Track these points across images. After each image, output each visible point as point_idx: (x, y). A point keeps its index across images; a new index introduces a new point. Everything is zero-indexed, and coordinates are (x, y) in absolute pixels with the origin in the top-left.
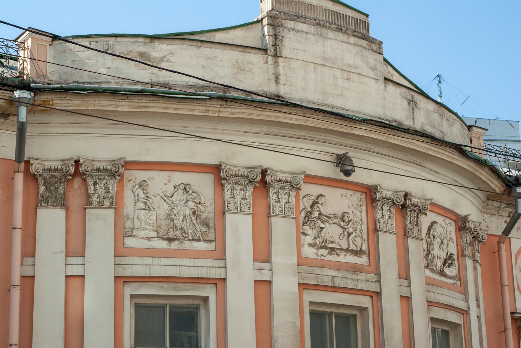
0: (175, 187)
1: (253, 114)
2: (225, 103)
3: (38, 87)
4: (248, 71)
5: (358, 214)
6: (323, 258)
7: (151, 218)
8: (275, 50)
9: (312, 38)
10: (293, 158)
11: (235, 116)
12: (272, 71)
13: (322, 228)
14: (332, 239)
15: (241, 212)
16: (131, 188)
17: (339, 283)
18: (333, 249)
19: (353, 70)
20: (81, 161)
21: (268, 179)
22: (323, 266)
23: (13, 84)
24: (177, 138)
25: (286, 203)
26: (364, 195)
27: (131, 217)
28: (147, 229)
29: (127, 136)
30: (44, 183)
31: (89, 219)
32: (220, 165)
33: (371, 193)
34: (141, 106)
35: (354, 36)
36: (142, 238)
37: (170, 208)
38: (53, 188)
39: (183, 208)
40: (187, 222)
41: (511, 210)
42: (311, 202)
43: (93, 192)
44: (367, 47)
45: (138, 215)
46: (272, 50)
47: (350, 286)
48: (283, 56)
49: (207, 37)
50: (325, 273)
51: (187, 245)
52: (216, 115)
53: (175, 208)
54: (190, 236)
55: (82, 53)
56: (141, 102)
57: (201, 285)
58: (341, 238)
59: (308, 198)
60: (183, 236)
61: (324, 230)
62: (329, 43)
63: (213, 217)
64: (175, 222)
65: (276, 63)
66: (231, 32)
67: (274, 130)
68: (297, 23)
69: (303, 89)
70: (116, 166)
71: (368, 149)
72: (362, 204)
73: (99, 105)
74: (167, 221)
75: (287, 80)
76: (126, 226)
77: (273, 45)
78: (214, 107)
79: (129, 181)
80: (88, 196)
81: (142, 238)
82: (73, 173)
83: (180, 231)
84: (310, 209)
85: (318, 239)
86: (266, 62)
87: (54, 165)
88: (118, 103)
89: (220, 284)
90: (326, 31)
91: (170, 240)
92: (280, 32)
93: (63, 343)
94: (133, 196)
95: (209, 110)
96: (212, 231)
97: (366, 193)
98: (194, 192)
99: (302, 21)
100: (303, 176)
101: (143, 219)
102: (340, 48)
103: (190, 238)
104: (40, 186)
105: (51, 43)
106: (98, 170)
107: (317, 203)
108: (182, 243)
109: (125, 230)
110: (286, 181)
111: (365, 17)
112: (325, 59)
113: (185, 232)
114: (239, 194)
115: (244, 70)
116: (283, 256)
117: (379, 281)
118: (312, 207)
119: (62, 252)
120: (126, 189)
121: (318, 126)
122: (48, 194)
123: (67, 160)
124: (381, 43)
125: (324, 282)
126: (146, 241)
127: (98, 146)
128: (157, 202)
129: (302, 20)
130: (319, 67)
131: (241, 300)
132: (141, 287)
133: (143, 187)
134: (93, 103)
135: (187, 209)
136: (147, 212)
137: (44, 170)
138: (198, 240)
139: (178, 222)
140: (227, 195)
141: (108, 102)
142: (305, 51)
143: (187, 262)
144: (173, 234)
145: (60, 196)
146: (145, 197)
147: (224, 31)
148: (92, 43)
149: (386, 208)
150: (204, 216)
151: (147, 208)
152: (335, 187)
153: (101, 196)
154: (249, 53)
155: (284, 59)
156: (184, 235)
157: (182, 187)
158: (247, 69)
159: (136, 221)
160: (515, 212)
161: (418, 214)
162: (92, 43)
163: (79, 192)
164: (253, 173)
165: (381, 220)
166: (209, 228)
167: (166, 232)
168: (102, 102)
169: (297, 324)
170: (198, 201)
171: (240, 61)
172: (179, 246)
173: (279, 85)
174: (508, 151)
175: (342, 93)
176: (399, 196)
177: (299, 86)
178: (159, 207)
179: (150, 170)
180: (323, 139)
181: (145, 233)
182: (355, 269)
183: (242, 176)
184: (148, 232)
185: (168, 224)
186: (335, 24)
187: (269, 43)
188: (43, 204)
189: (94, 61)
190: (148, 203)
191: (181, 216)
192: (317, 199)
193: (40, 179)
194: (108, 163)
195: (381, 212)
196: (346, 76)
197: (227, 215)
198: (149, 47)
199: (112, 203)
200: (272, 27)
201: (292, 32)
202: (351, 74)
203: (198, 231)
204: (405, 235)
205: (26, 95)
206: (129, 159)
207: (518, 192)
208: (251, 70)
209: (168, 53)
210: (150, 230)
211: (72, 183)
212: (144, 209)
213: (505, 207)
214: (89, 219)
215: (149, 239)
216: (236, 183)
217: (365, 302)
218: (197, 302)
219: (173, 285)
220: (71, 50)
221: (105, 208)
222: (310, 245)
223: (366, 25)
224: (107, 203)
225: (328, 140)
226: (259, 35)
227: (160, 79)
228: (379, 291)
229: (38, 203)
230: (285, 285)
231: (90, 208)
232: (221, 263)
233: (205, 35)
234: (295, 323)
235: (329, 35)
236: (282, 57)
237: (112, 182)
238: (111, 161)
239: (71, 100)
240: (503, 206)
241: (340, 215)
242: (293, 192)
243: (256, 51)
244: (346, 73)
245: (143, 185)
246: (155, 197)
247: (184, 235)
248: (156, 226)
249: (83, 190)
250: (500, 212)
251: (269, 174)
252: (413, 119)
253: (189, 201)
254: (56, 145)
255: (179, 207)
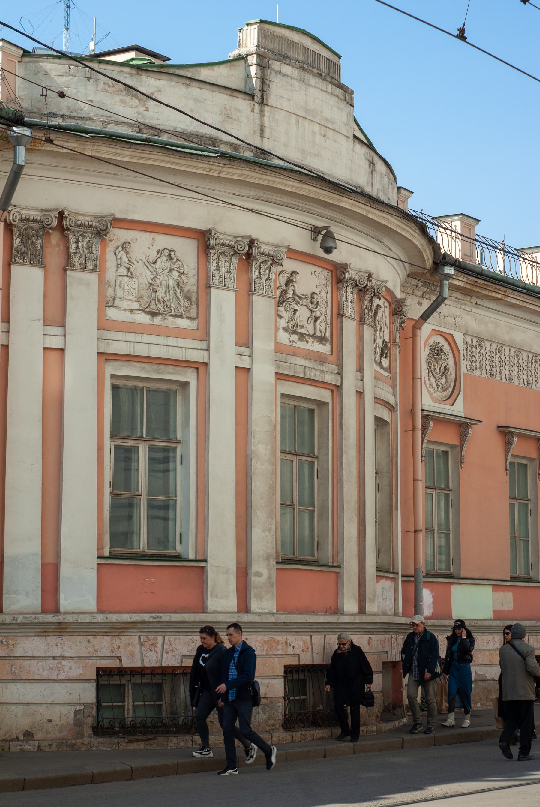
0: (158, 252)
1: (253, 177)
2: (229, 163)
3: (33, 123)
4: (235, 120)
5: (324, 295)
6: (295, 345)
7: (134, 286)
8: (262, 97)
9: (296, 83)
10: (278, 229)
11: (235, 178)
12: (258, 122)
13: (296, 311)
14: (302, 324)
15: (225, 287)
16: (113, 250)
17: (310, 374)
18: (302, 335)
19: (329, 125)
20: (66, 214)
21: (255, 251)
22: (295, 355)
23: (7, 116)
24: (166, 195)
25: (267, 280)
26: (330, 273)
27: (113, 284)
28: (130, 300)
29: (114, 188)
30: (20, 235)
31: (70, 283)
32: (209, 232)
33: (338, 274)
34: (142, 158)
35: (332, 83)
36: (125, 310)
37: (152, 276)
38: (29, 242)
39: (166, 278)
40: (170, 295)
41: (425, 289)
42: (285, 279)
43: (74, 251)
44: (342, 97)
45: (120, 283)
46: (259, 96)
47: (319, 378)
48: (270, 104)
49: (192, 72)
50: (296, 362)
51: (170, 321)
52: (217, 175)
53: (158, 277)
54: (173, 311)
55: (59, 77)
56: (144, 153)
57: (182, 369)
58: (309, 322)
59: (284, 275)
60: (165, 311)
61: (298, 313)
62: (311, 90)
63: (195, 290)
64: (158, 293)
65: (262, 111)
66: (216, 68)
67: (262, 195)
68: (283, 64)
69: (285, 145)
70: (104, 223)
71: (342, 222)
72: (328, 283)
73: (97, 151)
74: (149, 291)
75: (271, 133)
76: (108, 294)
77: (260, 90)
78: (218, 166)
79: (111, 241)
80: (68, 256)
81: (125, 310)
82: (55, 226)
83: (162, 305)
84: (284, 288)
85: (292, 323)
86: (253, 111)
87: (32, 214)
88: (119, 151)
89: (202, 369)
90: (308, 76)
91: (154, 314)
92: (268, 75)
93: (41, 426)
94: (115, 259)
95: (211, 169)
96: (194, 306)
97: (332, 271)
98: (178, 260)
99: (287, 62)
100: (286, 250)
101: (126, 287)
102: (315, 95)
103: (173, 313)
104: (15, 238)
105: (20, 60)
106: (82, 225)
107: (292, 281)
108: (165, 319)
109: (107, 299)
110: (269, 255)
111: (336, 58)
112: (307, 111)
113: (167, 306)
114: (224, 266)
115: (231, 118)
116: (262, 344)
117: (340, 373)
118: (287, 284)
119: (39, 320)
120: (108, 249)
121: (310, 195)
122: (24, 249)
123: (49, 211)
124: (352, 92)
125: (297, 373)
126: (129, 313)
127: (84, 195)
128: (139, 268)
129: (288, 61)
130: (301, 119)
131: (222, 385)
132: (123, 366)
133: (126, 250)
134: (91, 148)
135: (170, 279)
136: (130, 279)
137: (21, 219)
138: (181, 316)
139: (161, 294)
140: (213, 266)
141: (108, 149)
142: (289, 100)
143: (171, 341)
144: (155, 307)
145: (38, 253)
146: (128, 262)
147: (209, 67)
148: (72, 67)
149: (349, 290)
150: (186, 289)
151: (129, 274)
152: (308, 263)
153: (84, 257)
154: (237, 97)
155: (269, 107)
156: (166, 309)
157: (166, 253)
158: (234, 117)
159: (118, 289)
160: (440, 295)
161: (372, 297)
162: (72, 67)
163: (57, 249)
164: (241, 243)
165: (258, 281)
166: (191, 302)
167: (148, 304)
168: (101, 148)
169: (272, 419)
170: (182, 271)
171: (228, 107)
172: (163, 322)
173: (264, 139)
174: (423, 217)
175: (319, 152)
176: (363, 278)
177: (287, 142)
178: (141, 274)
179: (133, 230)
180: (306, 208)
181: (128, 305)
182: (320, 359)
183: (229, 246)
184: (131, 303)
185: (150, 295)
186: (317, 69)
187: (257, 87)
188: (18, 260)
189: (74, 90)
190: (132, 269)
191: (163, 287)
192: (292, 276)
193: (15, 230)
194: (93, 219)
195: (257, 271)
196: (323, 132)
197: (213, 291)
198: (135, 80)
199: (95, 266)
200: (260, 68)
201: (279, 76)
202: (327, 129)
203: (181, 306)
204: (361, 321)
205: (27, 132)
206: (118, 216)
207: (445, 272)
208: (238, 120)
209: (156, 90)
210: (133, 301)
211: (50, 238)
212: (127, 276)
213: (422, 286)
214: (70, 283)
215: (131, 311)
216: (221, 254)
217: (325, 395)
218: (174, 387)
219: (155, 367)
220: (46, 72)
221: (89, 272)
222: (286, 329)
223: (338, 68)
224: (90, 266)
225: (310, 209)
226: (242, 74)
227: (147, 121)
228: (340, 385)
229: (11, 259)
230: (263, 373)
231: (72, 270)
232: (204, 345)
233: (191, 70)
234: (271, 417)
235: (311, 81)
236: (268, 105)
237: (95, 240)
238: (97, 217)
239: (67, 142)
240: (420, 284)
241: (309, 295)
242: (274, 268)
243: (243, 96)
244: (323, 128)
245: (125, 246)
246: (138, 262)
247: (166, 309)
248: (138, 297)
249: (62, 247)
250: (415, 291)
251: (256, 246)
252: (372, 184)
253: (173, 270)
254: (43, 191)
255: (162, 276)
